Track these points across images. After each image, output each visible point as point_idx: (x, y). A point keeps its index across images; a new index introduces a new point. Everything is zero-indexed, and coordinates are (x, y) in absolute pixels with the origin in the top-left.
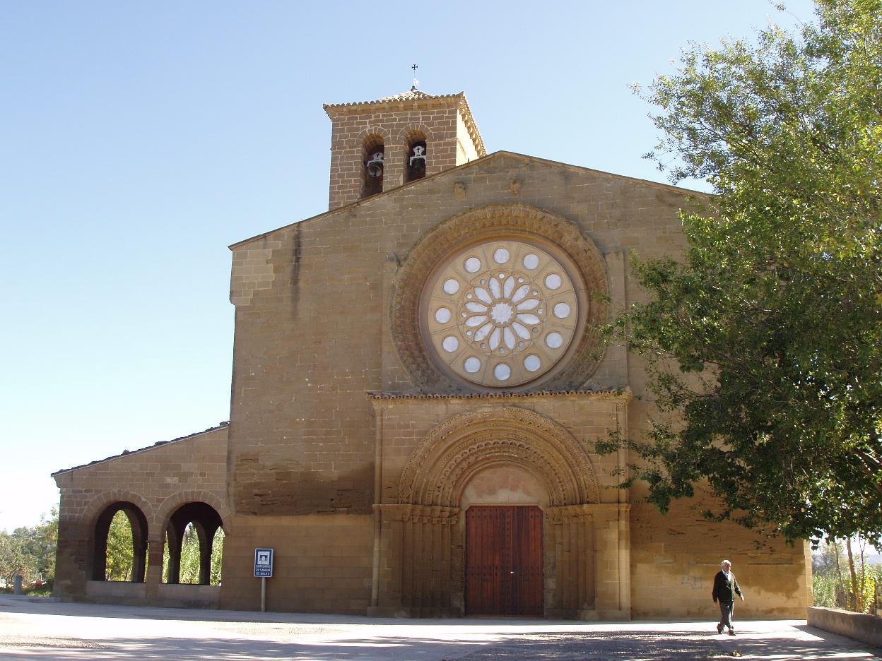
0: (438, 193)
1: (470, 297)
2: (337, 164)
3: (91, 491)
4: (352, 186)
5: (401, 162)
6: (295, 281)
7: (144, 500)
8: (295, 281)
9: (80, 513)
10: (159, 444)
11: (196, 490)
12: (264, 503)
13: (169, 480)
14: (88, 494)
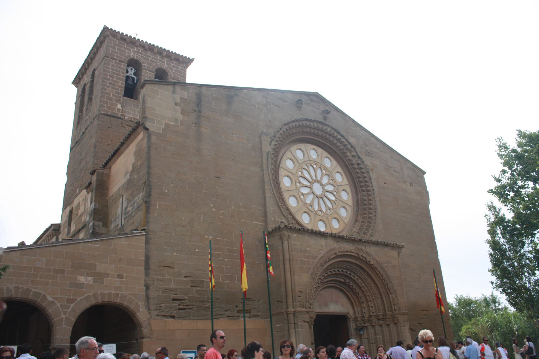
2: (109, 67)
4: (119, 86)
7: (50, 299)
11: (113, 292)
12: (181, 307)
13: (82, 279)
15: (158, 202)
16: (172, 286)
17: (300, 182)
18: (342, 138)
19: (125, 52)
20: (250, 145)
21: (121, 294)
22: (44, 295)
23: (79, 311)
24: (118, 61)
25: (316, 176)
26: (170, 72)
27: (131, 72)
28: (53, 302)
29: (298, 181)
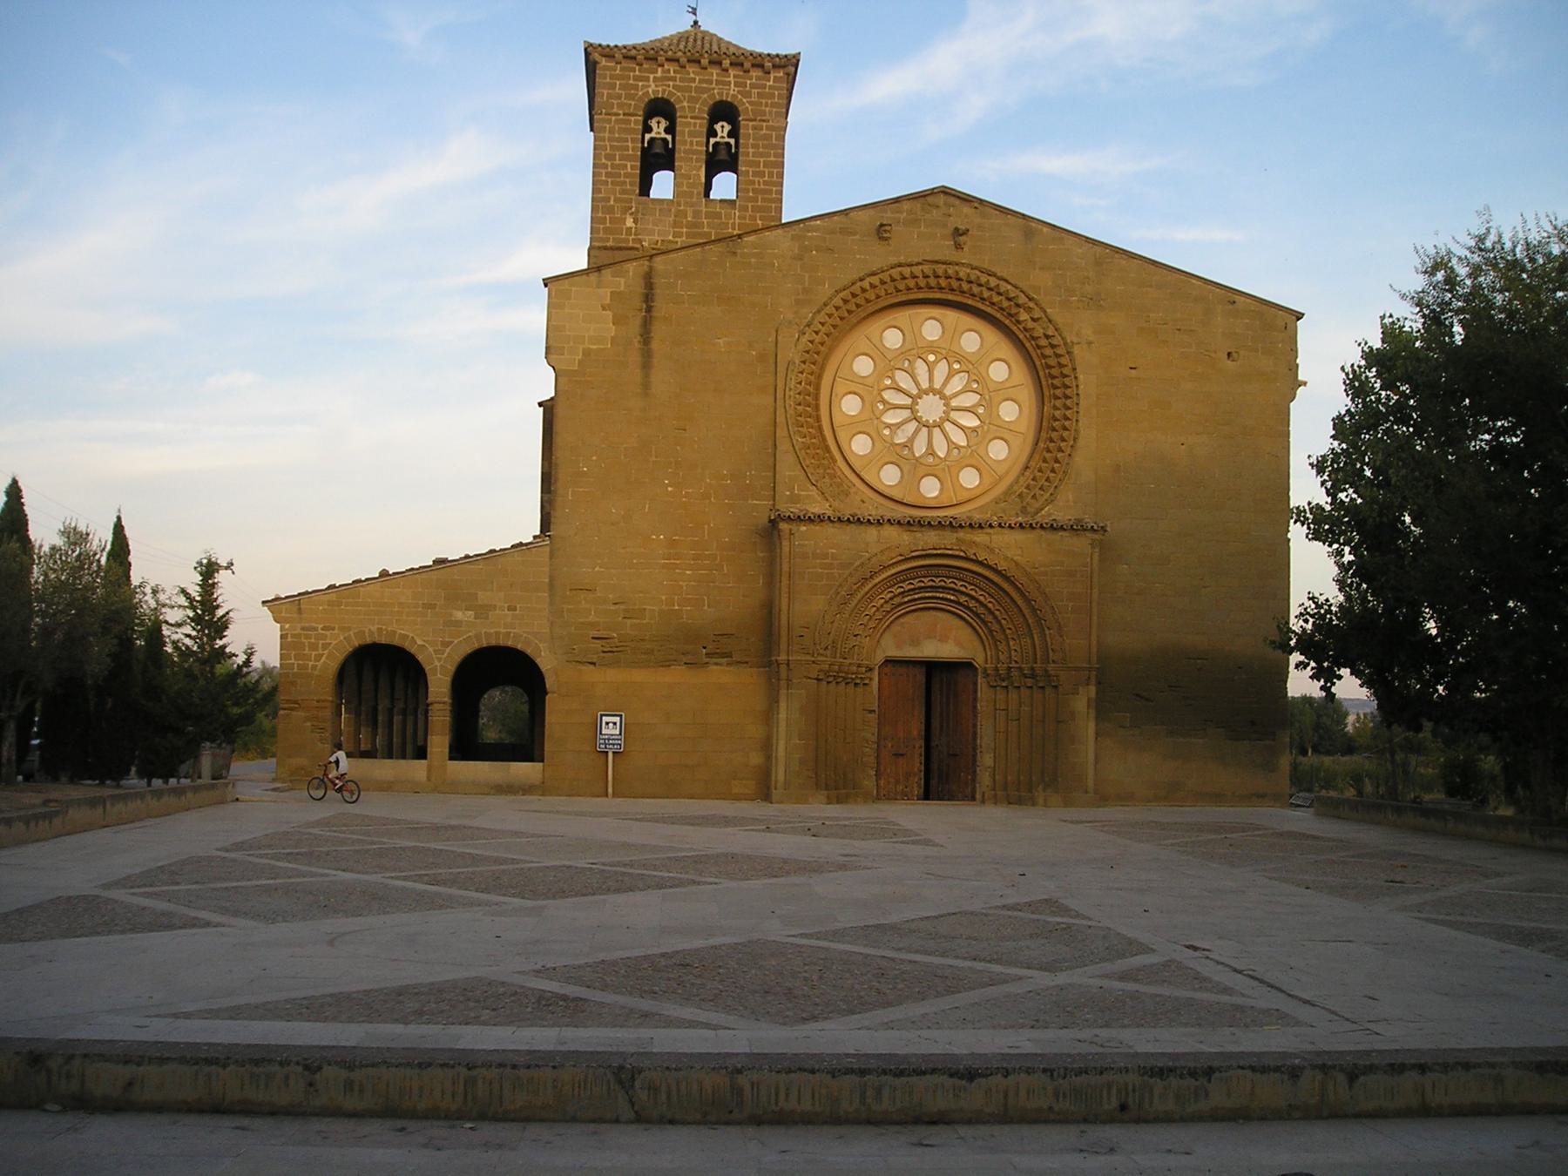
0: (854, 235)
1: (888, 382)
3: (333, 629)
4: (627, 175)
5: (702, 146)
6: (646, 337)
8: (646, 337)
9: (316, 660)
10: (438, 562)
13: (459, 615)
14: (328, 633)
15: (570, 490)
16: (592, 618)
17: (884, 402)
18: (1002, 283)
19: (636, 88)
20: (754, 353)
21: (514, 633)
22: (413, 637)
23: (458, 659)
24: (621, 117)
25: (931, 380)
26: (744, 104)
27: (658, 127)
28: (424, 646)
29: (879, 398)
